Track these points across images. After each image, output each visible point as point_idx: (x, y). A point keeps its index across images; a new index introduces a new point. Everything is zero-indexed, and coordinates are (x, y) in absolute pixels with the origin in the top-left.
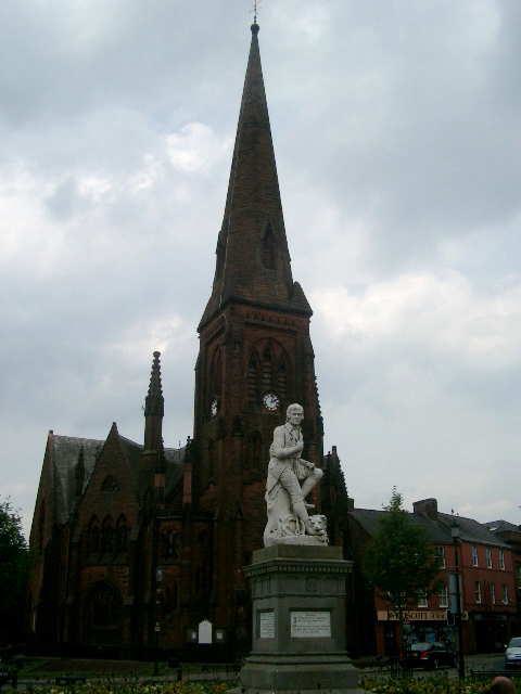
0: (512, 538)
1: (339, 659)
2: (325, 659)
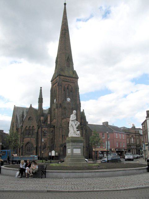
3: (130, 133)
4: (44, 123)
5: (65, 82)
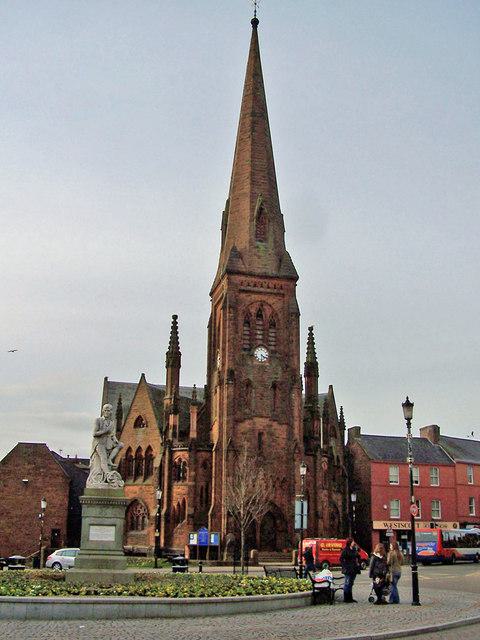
5: (257, 295)
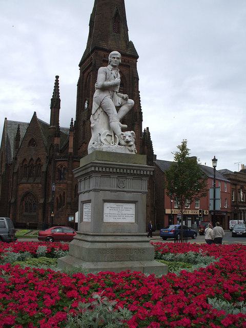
0: (231, 177)
1: (140, 239)
2: (130, 239)
3: (239, 181)
4: (61, 152)
